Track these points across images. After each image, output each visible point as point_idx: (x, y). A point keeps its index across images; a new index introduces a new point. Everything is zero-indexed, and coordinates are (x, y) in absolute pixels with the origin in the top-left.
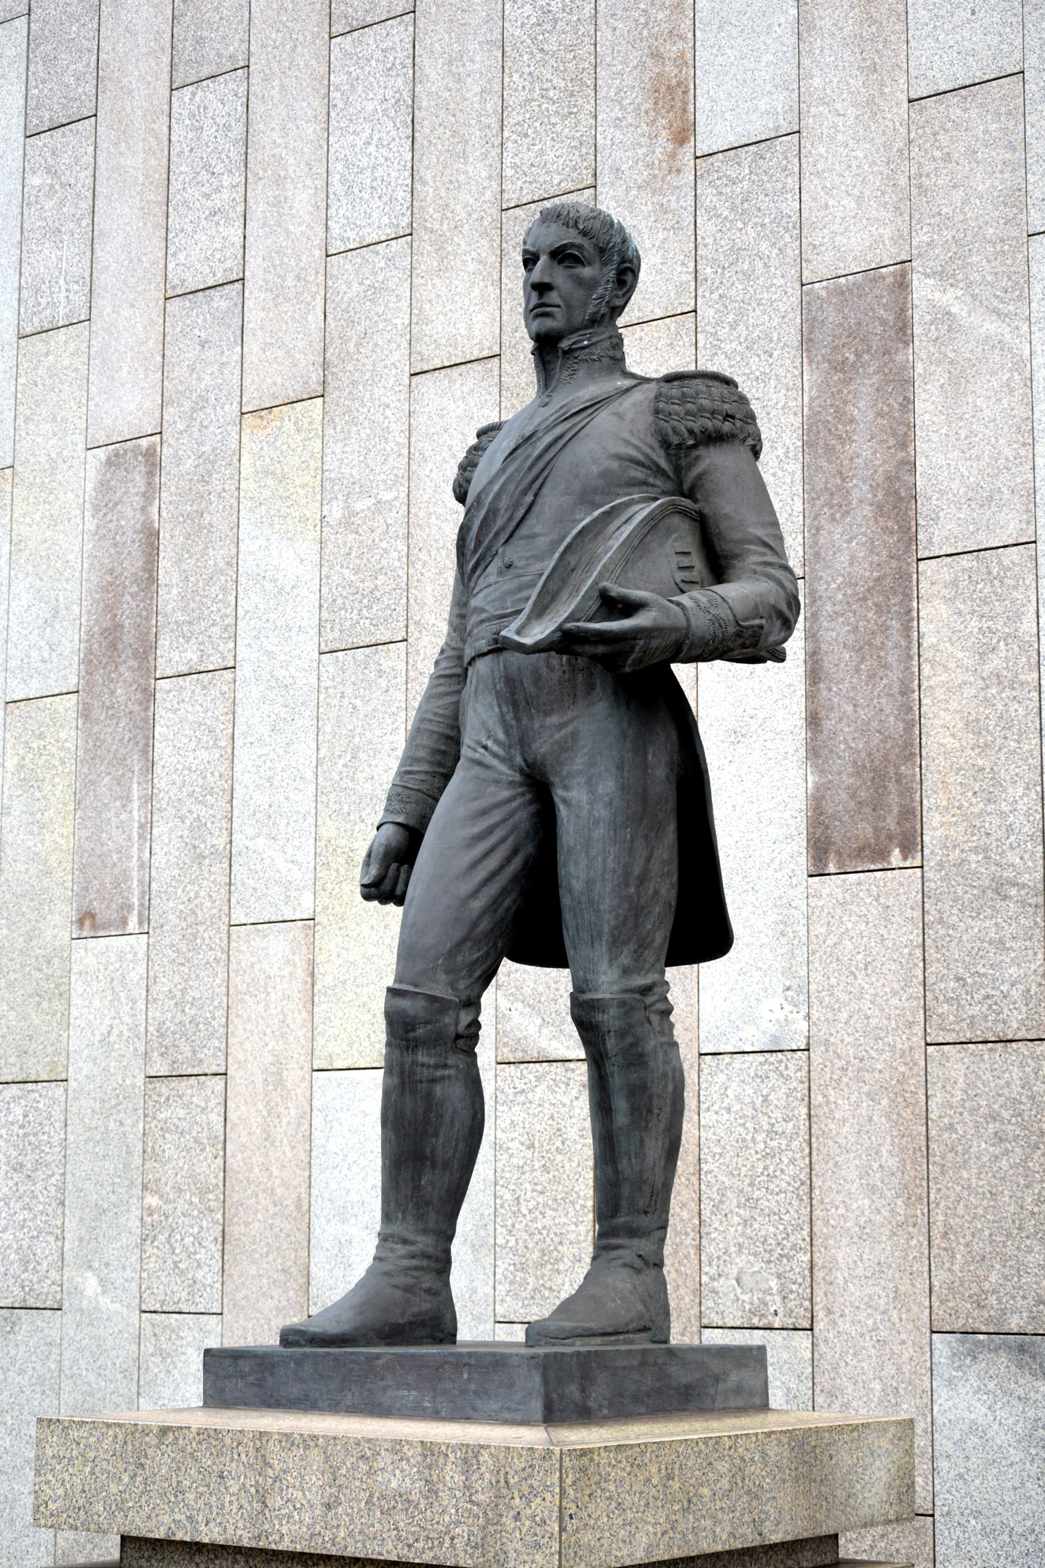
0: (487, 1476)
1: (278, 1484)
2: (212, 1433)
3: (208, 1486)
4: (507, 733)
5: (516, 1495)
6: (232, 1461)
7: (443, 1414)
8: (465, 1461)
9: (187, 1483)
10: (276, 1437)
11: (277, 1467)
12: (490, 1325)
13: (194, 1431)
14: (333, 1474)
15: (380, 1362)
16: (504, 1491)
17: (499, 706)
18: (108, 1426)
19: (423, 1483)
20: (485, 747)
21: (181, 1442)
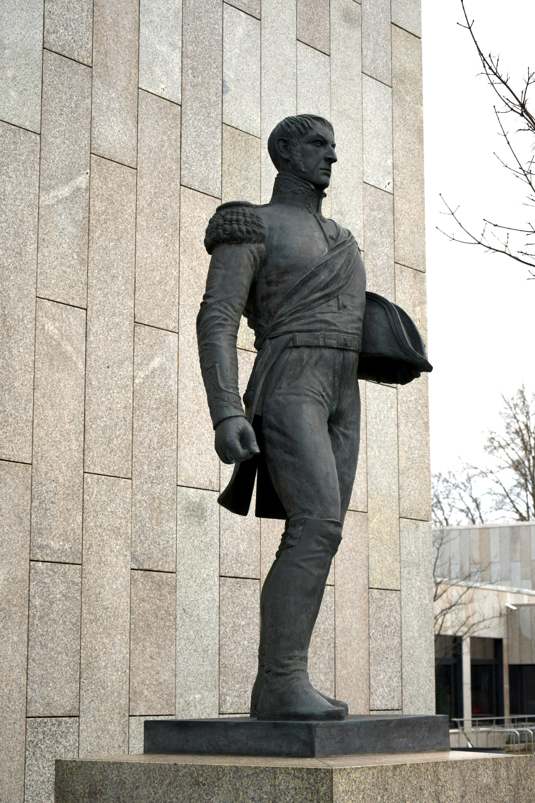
0: (514, 771)
1: (443, 789)
2: (416, 766)
3: (415, 796)
4: (334, 392)
5: (523, 779)
6: (425, 780)
7: (416, 749)
8: (507, 765)
9: (407, 796)
10: (442, 764)
11: (442, 780)
12: (218, 714)
13: (408, 766)
14: (463, 779)
15: (392, 725)
16: (519, 777)
17: (334, 377)
18: (369, 768)
19: (494, 778)
20: (323, 396)
21: (403, 773)
